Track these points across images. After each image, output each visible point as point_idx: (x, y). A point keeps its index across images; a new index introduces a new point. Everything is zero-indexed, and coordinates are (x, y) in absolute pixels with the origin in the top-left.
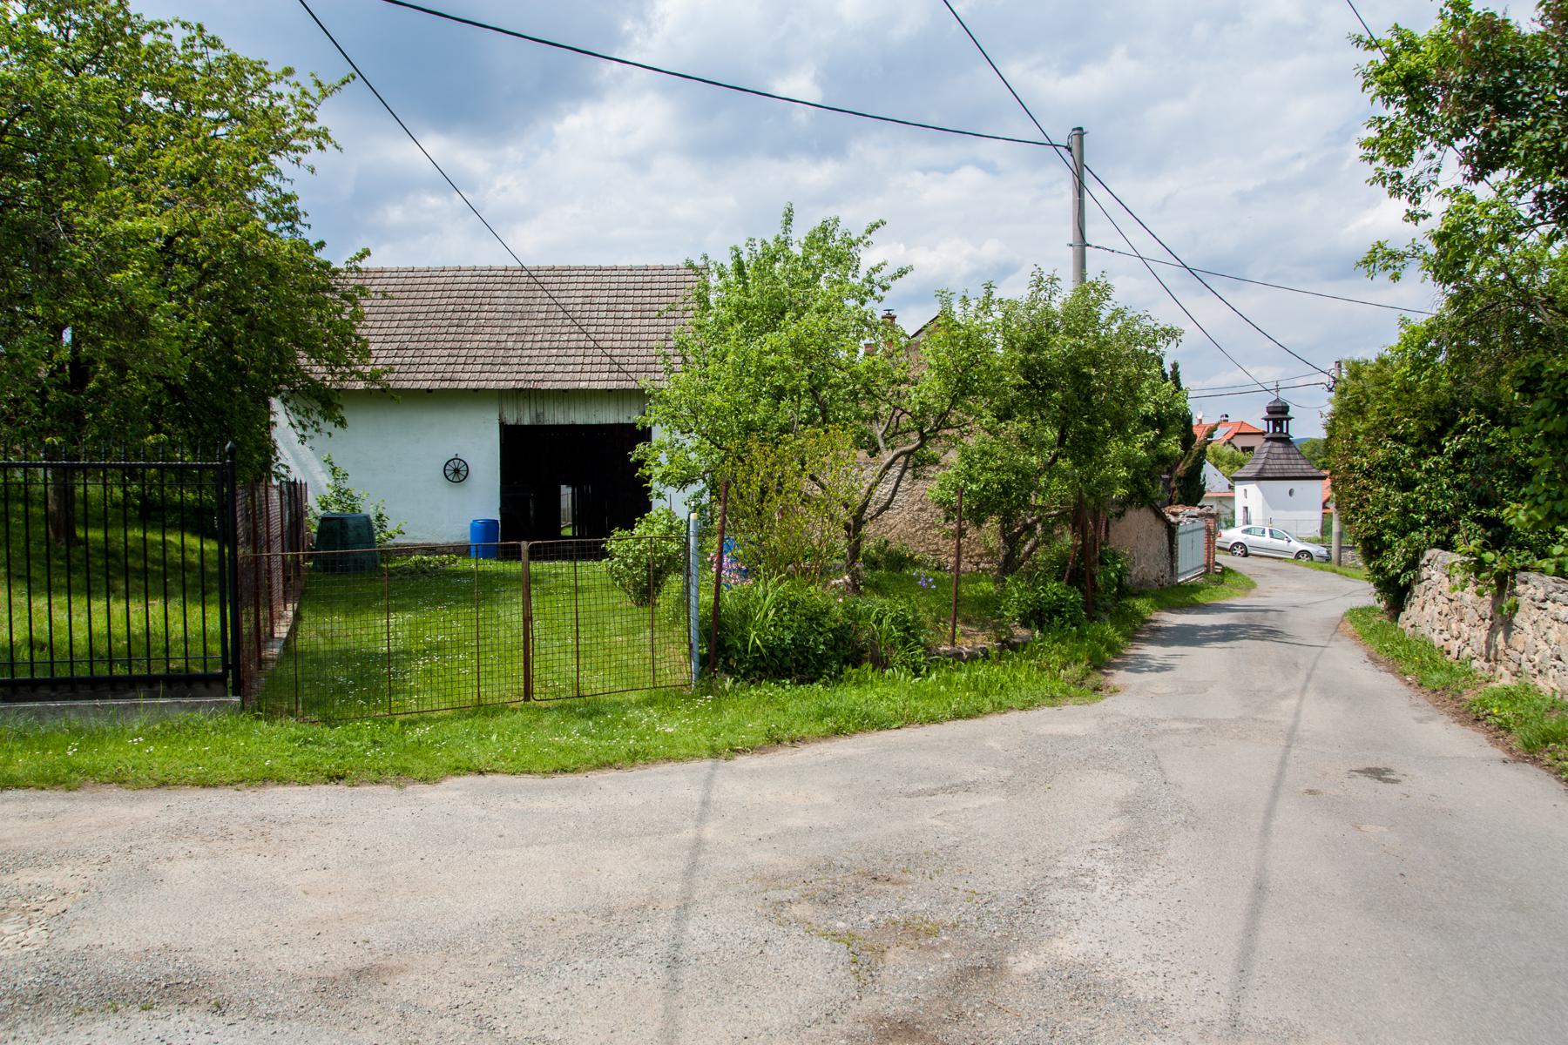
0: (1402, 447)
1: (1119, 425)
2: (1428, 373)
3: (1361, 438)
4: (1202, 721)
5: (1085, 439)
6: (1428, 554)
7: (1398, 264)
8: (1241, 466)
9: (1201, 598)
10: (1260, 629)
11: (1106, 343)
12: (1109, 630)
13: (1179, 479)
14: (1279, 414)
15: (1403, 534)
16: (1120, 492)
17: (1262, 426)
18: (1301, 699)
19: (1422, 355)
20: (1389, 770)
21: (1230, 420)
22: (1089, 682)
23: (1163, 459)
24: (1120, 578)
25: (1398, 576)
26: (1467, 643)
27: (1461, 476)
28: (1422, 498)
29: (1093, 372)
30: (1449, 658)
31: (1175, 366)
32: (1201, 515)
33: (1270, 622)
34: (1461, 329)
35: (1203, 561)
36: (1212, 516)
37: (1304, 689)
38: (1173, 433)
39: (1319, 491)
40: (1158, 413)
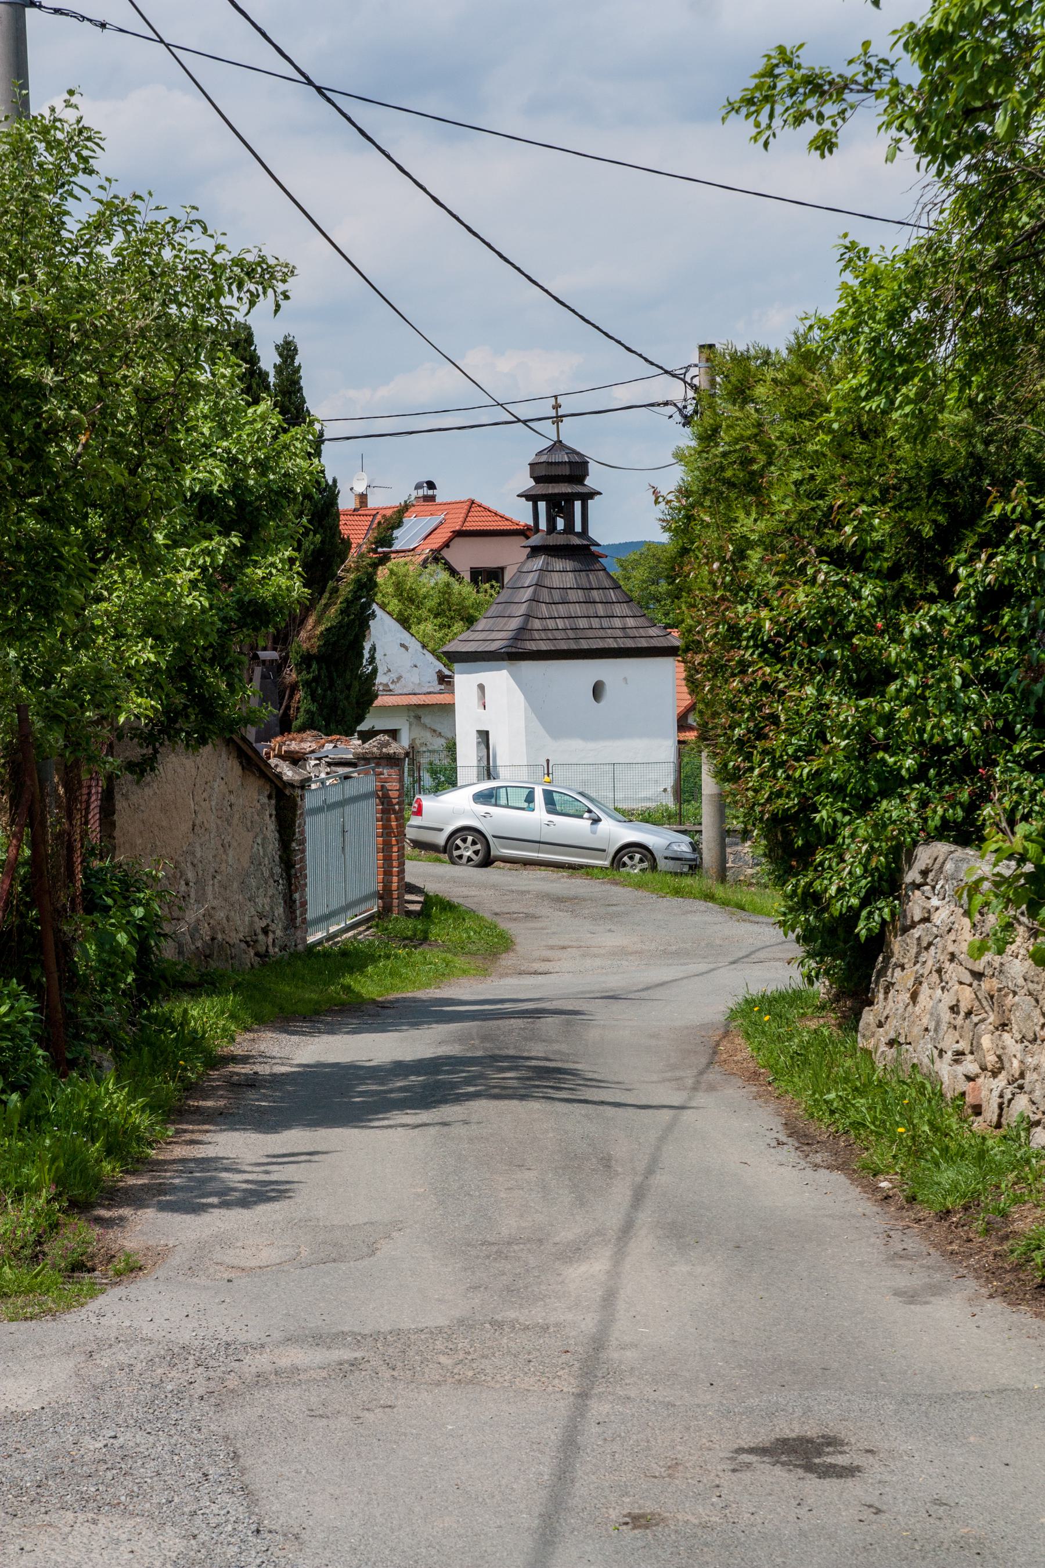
0: (854, 579)
1: (128, 528)
2: (910, 390)
3: (755, 556)
4: (359, 1339)
5: (31, 565)
6: (924, 855)
7: (830, 109)
8: (470, 621)
9: (368, 986)
10: (520, 1066)
11: (82, 295)
12: (113, 1096)
13: (307, 660)
14: (562, 481)
15: (864, 804)
16: (138, 706)
17: (521, 514)
18: (619, 1257)
19: (897, 342)
20: (833, 1442)
21: (442, 495)
22: (54, 1249)
23: (255, 613)
24: (144, 949)
25: (852, 917)
26: (1018, 1083)
27: (996, 653)
28: (904, 713)
29: (49, 377)
30: (979, 1124)
31: (288, 350)
32: (361, 760)
33: (544, 1045)
34: (985, 277)
35: (374, 883)
36: (393, 761)
37: (627, 1229)
38: (280, 539)
39: (657, 688)
40: (238, 487)
